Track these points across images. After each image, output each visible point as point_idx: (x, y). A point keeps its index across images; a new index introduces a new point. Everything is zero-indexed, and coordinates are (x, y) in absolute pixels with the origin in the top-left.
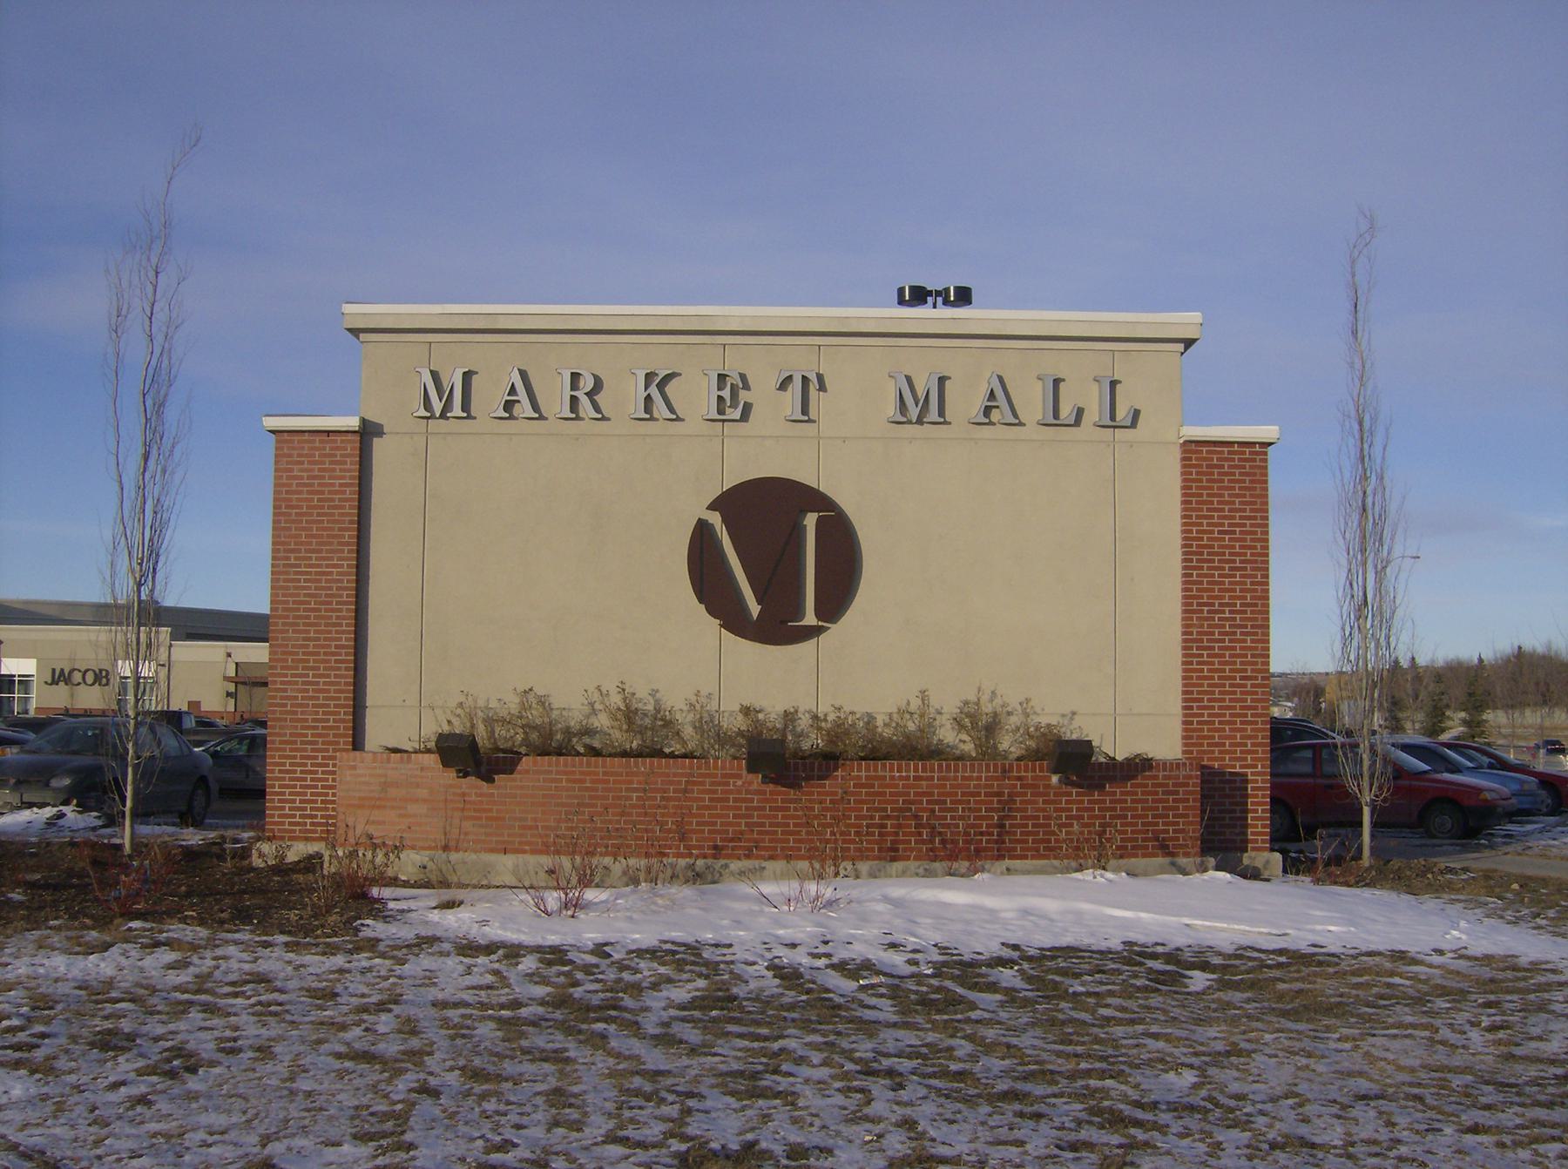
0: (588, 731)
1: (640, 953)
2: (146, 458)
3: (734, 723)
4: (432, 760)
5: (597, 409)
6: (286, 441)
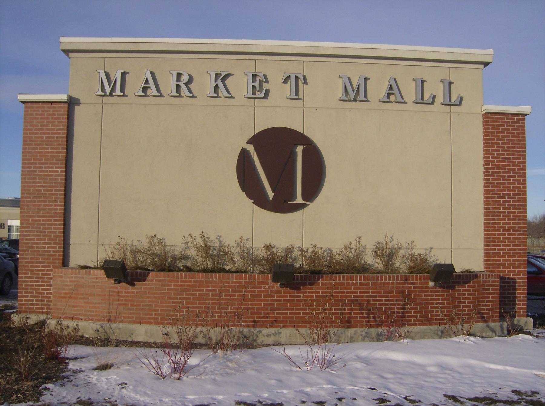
0: (184, 258)
3: (261, 253)
5: (190, 91)
6: (29, 107)
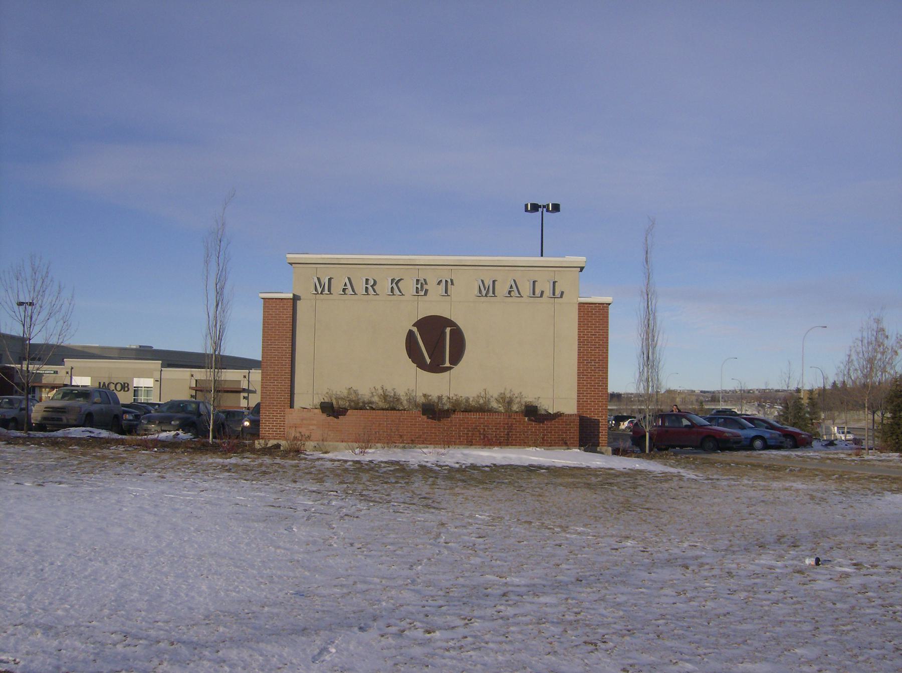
0: (371, 402)
1: (382, 462)
2: (217, 305)
3: (421, 400)
4: (318, 411)
5: (375, 291)
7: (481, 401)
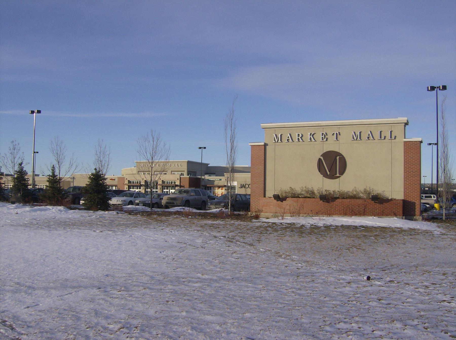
5: (302, 140)
7: (355, 193)
